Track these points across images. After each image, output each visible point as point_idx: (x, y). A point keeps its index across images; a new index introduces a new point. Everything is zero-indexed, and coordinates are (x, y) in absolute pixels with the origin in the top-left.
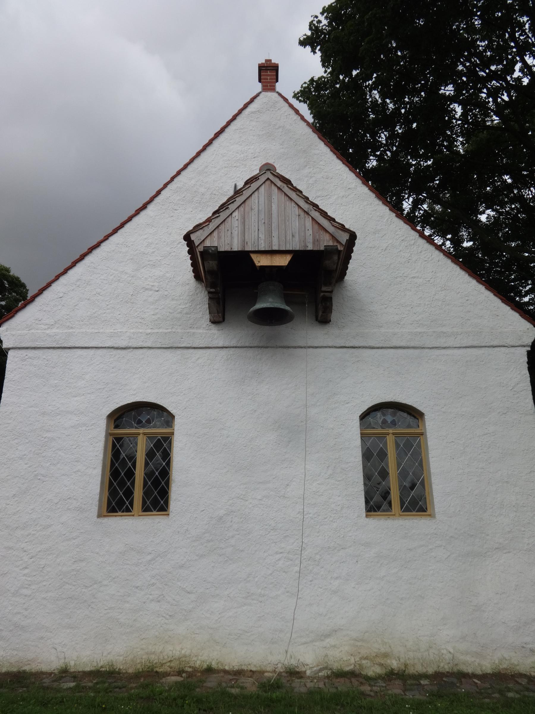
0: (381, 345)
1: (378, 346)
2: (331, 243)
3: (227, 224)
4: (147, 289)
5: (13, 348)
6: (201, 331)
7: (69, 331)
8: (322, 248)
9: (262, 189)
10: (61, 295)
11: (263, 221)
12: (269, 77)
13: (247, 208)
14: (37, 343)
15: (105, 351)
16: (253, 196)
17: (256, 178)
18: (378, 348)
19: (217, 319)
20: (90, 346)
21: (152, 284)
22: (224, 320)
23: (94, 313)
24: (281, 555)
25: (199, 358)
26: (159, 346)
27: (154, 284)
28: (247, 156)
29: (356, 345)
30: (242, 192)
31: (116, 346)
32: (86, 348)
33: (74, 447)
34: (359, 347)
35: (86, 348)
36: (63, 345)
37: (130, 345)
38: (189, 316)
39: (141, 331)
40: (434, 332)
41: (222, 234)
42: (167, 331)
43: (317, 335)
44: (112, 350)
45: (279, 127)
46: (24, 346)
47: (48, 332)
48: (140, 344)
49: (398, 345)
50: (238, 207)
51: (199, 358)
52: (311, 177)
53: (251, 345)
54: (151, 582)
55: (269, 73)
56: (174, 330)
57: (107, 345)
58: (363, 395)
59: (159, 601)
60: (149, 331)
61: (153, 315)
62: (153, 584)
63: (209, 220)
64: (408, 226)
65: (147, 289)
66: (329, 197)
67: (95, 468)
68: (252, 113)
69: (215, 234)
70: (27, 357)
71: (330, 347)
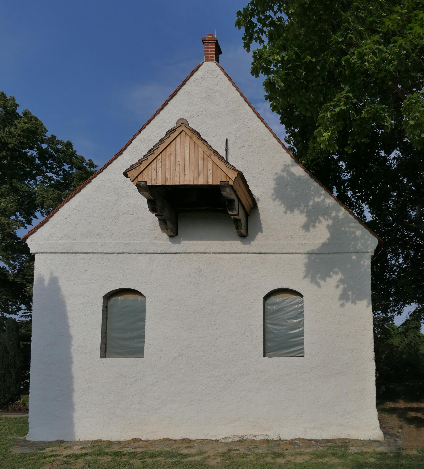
0: (279, 252)
1: (277, 252)
2: (224, 180)
3: (154, 165)
4: (125, 213)
5: (37, 253)
6: (161, 242)
7: (74, 241)
8: (219, 184)
9: (178, 139)
10: (67, 217)
11: (179, 163)
12: (210, 50)
13: (168, 153)
14: (53, 250)
15: (99, 255)
16: (172, 143)
17: (174, 130)
18: (278, 254)
19: (172, 234)
20: (88, 252)
21: (128, 209)
22: (177, 234)
23: (90, 230)
24: (212, 378)
25: (161, 260)
26: (134, 252)
27: (130, 209)
28: (193, 114)
29: (263, 252)
30: (164, 141)
31: (105, 252)
32: (86, 253)
33: (83, 316)
34: (266, 253)
35: (86, 253)
36: (70, 251)
37: (115, 251)
38: (154, 231)
39: (121, 242)
40: (313, 243)
41: (150, 173)
42: (139, 242)
43: (237, 245)
44: (104, 254)
45: (217, 91)
46: (44, 251)
47: (59, 242)
48: (121, 251)
49: (290, 252)
50: (161, 152)
51: (161, 260)
52: (238, 131)
53: (363, 254)
54: (135, 394)
55: (210, 46)
56: (143, 241)
57: (100, 252)
58: (266, 284)
59: (140, 404)
60: (127, 242)
61: (130, 231)
62: (136, 395)
63: (140, 162)
64: (302, 169)
65: (125, 213)
66: (250, 146)
67: (97, 329)
68: (197, 79)
69: (145, 172)
70: (47, 259)
71: (246, 253)
